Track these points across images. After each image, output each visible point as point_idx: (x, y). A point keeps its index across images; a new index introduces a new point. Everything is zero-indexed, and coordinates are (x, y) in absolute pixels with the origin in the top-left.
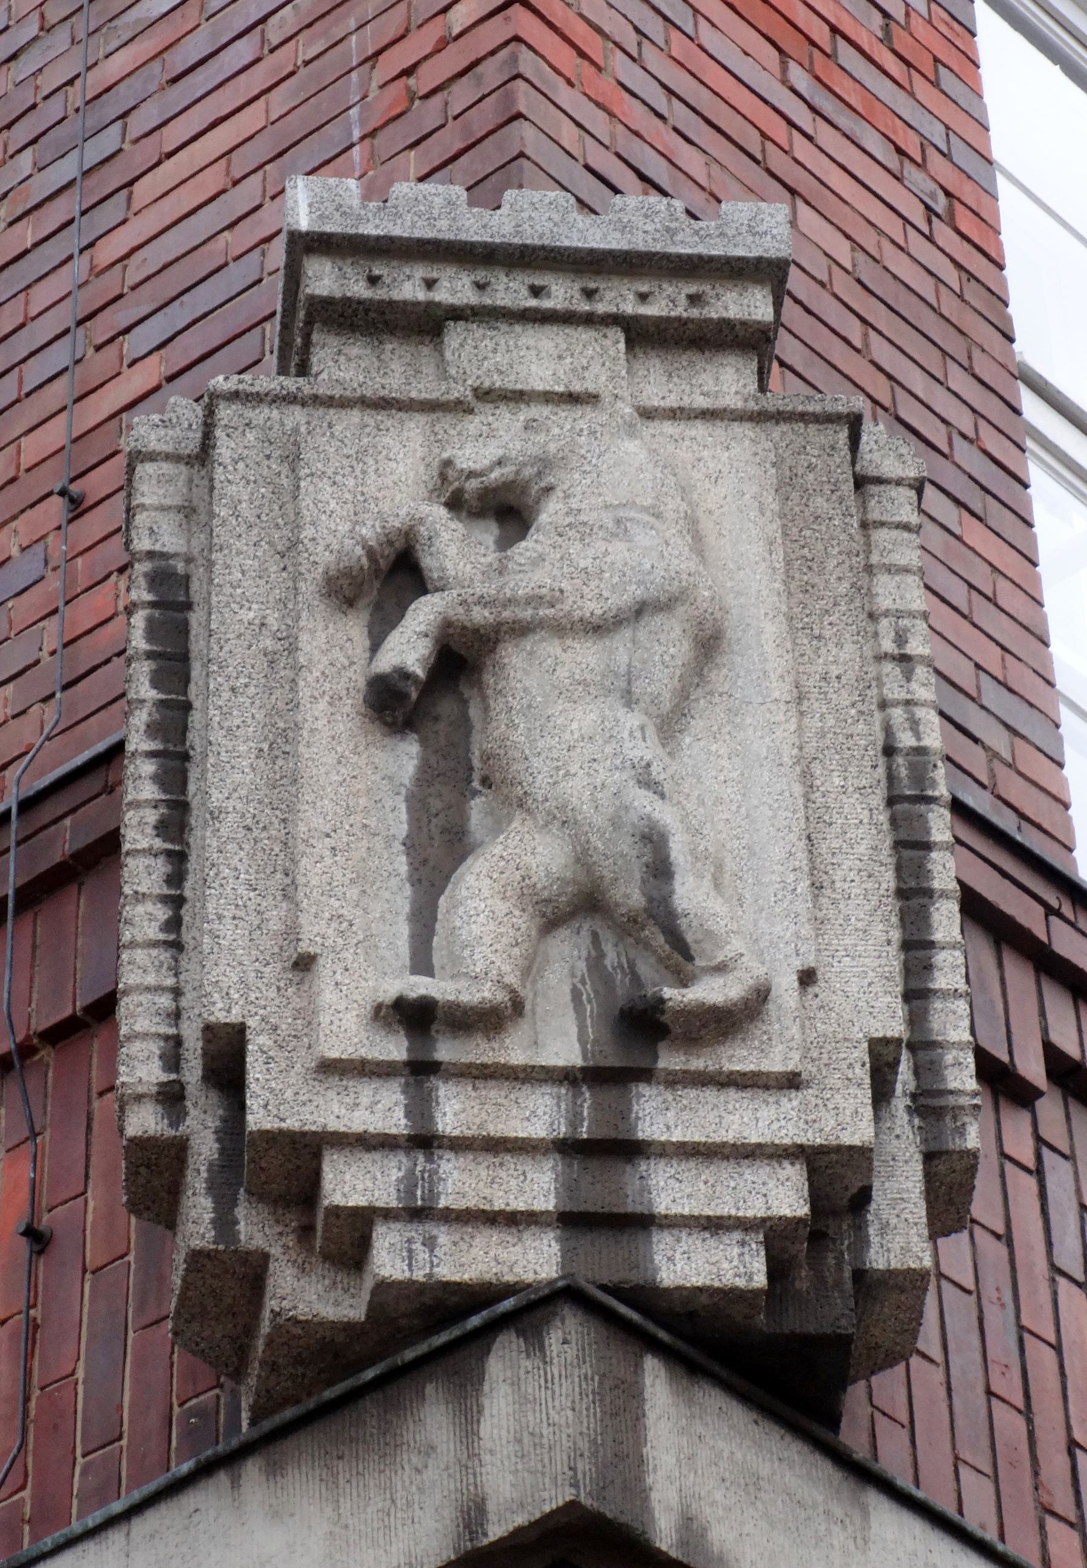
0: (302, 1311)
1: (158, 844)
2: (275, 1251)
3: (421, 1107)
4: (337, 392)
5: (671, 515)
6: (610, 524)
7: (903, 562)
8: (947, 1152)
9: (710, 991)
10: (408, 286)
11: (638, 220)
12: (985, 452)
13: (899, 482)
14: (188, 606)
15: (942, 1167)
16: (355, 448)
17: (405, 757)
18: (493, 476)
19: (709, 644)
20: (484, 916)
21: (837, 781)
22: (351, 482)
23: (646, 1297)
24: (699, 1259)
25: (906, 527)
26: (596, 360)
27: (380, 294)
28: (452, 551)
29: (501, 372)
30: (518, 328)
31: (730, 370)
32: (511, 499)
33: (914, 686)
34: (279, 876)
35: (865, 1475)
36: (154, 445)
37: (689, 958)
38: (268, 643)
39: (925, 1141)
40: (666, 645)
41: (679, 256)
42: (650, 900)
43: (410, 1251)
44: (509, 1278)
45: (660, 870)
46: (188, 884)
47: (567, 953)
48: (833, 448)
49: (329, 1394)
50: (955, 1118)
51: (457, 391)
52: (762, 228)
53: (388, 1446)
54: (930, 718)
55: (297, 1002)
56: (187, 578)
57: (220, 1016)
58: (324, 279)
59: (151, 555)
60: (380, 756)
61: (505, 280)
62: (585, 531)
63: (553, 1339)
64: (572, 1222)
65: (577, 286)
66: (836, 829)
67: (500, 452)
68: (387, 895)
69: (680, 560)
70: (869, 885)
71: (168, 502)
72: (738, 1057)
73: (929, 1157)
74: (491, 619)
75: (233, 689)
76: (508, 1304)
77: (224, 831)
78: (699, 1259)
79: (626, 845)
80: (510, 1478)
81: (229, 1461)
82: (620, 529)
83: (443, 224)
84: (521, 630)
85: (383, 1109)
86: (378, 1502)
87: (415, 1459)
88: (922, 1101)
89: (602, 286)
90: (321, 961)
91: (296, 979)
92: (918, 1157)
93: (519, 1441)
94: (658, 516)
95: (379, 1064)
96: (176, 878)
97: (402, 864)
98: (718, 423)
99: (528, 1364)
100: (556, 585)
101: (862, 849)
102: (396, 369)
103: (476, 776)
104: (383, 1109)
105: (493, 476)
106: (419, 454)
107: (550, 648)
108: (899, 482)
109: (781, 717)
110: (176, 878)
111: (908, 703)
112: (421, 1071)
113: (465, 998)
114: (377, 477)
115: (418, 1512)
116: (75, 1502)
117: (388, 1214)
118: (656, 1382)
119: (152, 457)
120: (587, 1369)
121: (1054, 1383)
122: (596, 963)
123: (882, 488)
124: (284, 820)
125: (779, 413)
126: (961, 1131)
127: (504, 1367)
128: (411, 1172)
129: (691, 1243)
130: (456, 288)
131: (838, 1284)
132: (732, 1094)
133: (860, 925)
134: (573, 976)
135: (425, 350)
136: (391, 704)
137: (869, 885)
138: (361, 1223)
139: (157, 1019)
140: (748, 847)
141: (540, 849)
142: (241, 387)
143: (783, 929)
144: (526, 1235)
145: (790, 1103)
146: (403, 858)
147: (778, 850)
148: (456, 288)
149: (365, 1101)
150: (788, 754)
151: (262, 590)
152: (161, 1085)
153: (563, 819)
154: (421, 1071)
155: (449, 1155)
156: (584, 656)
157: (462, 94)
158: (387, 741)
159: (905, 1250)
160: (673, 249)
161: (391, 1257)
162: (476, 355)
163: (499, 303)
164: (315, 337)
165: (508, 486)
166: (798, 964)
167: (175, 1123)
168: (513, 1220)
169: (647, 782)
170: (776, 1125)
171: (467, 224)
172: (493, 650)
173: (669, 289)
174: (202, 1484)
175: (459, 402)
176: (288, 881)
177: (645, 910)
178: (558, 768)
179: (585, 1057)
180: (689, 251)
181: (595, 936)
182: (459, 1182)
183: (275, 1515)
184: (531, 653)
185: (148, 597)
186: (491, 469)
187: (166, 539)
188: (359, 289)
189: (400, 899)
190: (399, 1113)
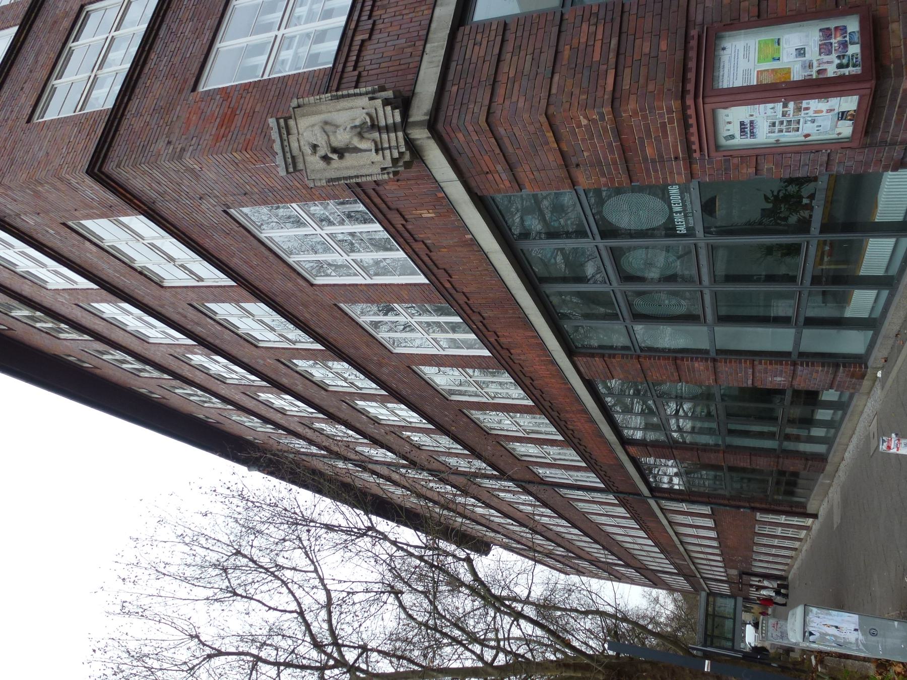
3: (386, 149)
9: (368, 120)
10: (290, 160)
17: (347, 155)
19: (326, 123)
20: (363, 145)
23: (402, 121)
26: (293, 139)
40: (327, 128)
45: (355, 127)
47: (366, 135)
58: (291, 170)
62: (317, 139)
64: (396, 131)
72: (374, 115)
81: (423, 161)
82: (316, 135)
85: (387, 152)
102: (300, 161)
104: (387, 152)
112: (383, 149)
114: (314, 162)
118: (411, 120)
130: (288, 155)
136: (341, 157)
138: (400, 153)
148: (288, 155)
153: (351, 138)
154: (383, 149)
156: (332, 138)
157: (258, 155)
161: (403, 149)
162: (296, 152)
182: (394, 143)
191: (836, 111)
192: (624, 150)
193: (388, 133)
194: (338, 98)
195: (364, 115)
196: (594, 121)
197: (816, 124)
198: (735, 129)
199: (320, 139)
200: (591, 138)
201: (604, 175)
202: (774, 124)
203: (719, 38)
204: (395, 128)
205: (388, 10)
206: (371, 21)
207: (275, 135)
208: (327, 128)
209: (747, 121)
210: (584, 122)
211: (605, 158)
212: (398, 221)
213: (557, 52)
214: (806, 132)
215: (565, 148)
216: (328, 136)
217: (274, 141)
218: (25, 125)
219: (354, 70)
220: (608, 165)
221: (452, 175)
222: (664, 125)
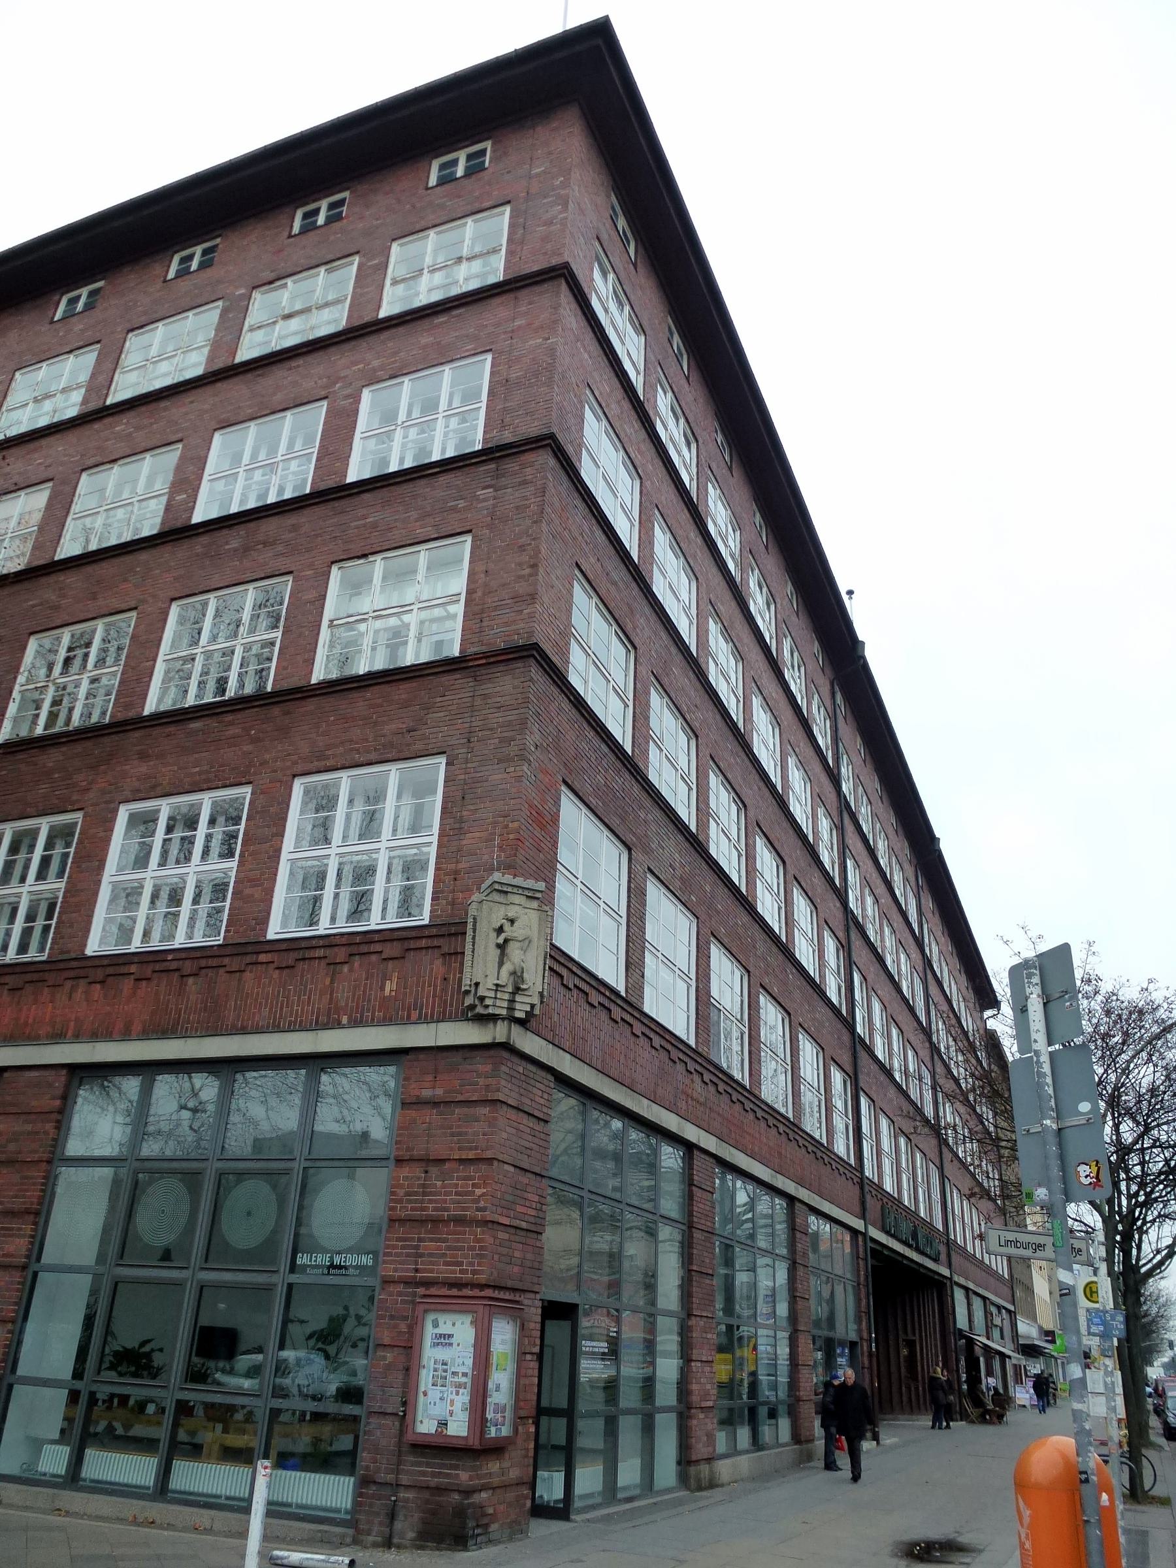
47: (512, 978)
58: (497, 886)
64: (508, 1008)
85: (492, 994)
104: (492, 994)
112: (496, 991)
127: (499, 1022)
130: (510, 889)
136: (498, 946)
147: (533, 969)
148: (510, 889)
154: (496, 991)
156: (518, 944)
161: (491, 1011)
182: (498, 1003)
191: (449, 1418)
192: (436, 1221)
196: (477, 1201)
197: (438, 1401)
198: (444, 1329)
200: (457, 1194)
201: (408, 1194)
202: (444, 1364)
203: (514, 1321)
204: (511, 1009)
207: (530, 883)
209: (452, 1340)
210: (478, 1192)
211: (430, 1201)
212: (390, 950)
213: (526, 1171)
214: (430, 1393)
215: (447, 1165)
218: (576, 558)
220: (422, 1202)
222: (460, 1264)
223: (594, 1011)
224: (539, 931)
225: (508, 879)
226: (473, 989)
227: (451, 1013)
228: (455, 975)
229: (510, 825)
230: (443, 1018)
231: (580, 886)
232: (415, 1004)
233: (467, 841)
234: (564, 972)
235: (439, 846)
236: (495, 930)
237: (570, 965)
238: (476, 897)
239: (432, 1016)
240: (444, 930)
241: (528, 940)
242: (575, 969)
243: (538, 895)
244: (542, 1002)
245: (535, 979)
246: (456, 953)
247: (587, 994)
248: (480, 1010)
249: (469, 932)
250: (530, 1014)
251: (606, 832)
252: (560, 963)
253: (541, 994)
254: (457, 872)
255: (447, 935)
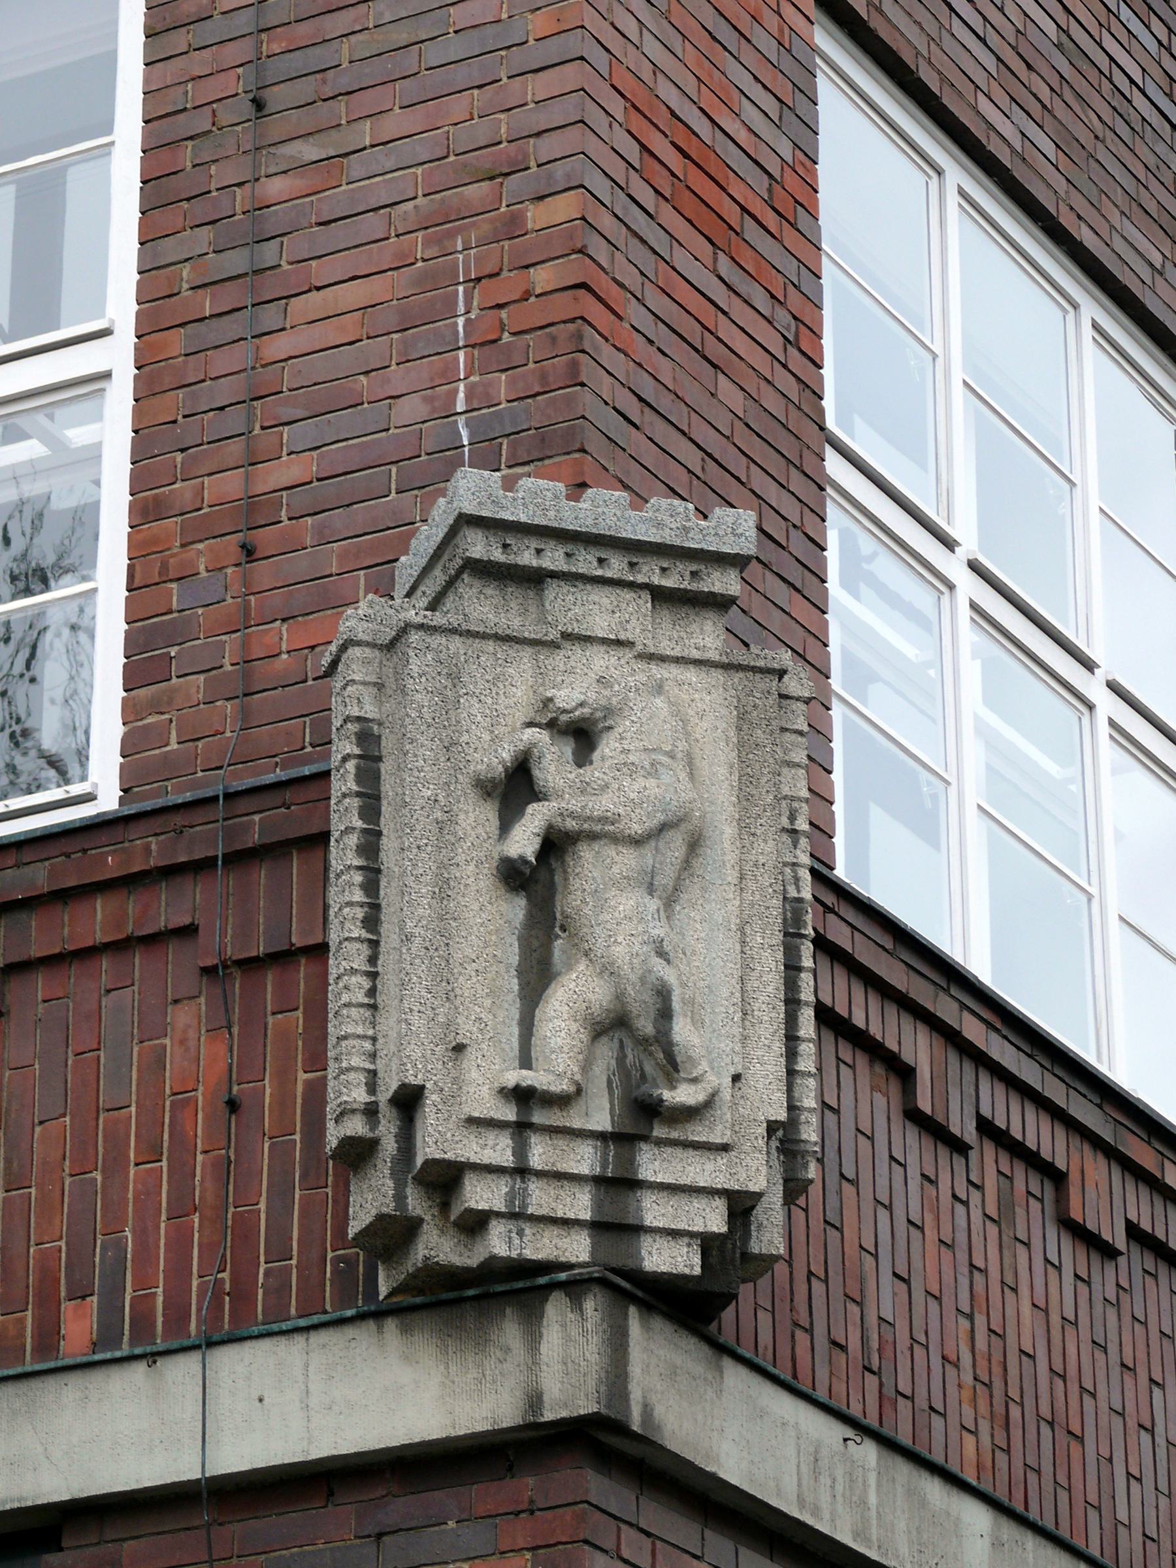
0: (442, 1258)
1: (365, 934)
2: (427, 1218)
3: (521, 1150)
4: (481, 629)
5: (680, 755)
6: (647, 764)
7: (797, 760)
8: (797, 1179)
9: (683, 1095)
11: (668, 520)
12: (806, 534)
13: (798, 699)
14: (379, 759)
15: (791, 1184)
16: (493, 675)
18: (577, 713)
19: (695, 845)
21: (759, 940)
22: (489, 701)
24: (666, 1254)
25: (801, 733)
26: (628, 615)
27: (511, 559)
28: (552, 768)
29: (577, 621)
30: (589, 587)
31: (710, 623)
32: (584, 726)
33: (798, 852)
34: (444, 984)
35: (722, 1349)
36: (361, 636)
37: (678, 1071)
38: (439, 814)
39: (785, 1171)
40: (674, 847)
41: (690, 548)
42: (658, 1032)
43: (510, 1238)
44: (563, 1259)
45: (665, 1014)
46: (379, 963)
47: (606, 1052)
48: (769, 692)
49: (444, 1296)
50: (803, 1157)
51: (553, 635)
52: (740, 531)
53: (481, 1343)
54: (806, 875)
55: (454, 1073)
56: (379, 737)
57: (411, 1080)
58: (478, 546)
59: (359, 719)
60: (504, 907)
61: (584, 553)
63: (589, 1305)
64: (598, 1227)
65: (626, 560)
66: (756, 974)
67: (583, 697)
68: (506, 1006)
69: (687, 792)
70: (773, 1015)
71: (368, 679)
72: (698, 1132)
73: (786, 1181)
74: (577, 827)
75: (419, 847)
76: (563, 1276)
77: (413, 950)
78: (666, 1254)
79: (648, 996)
80: (559, 1385)
82: (653, 771)
83: (552, 514)
84: (593, 837)
85: (497, 1150)
86: (473, 1374)
87: (498, 1353)
88: (786, 1146)
89: (641, 561)
90: (469, 1049)
91: (454, 1057)
92: (781, 1181)
93: (565, 1364)
94: (673, 757)
95: (500, 1121)
96: (373, 960)
97: (515, 985)
98: (703, 668)
99: (570, 1315)
100: (616, 811)
101: (770, 989)
103: (558, 924)
105: (577, 713)
106: (530, 683)
107: (610, 851)
108: (798, 699)
109: (731, 896)
110: (373, 960)
111: (794, 864)
112: (521, 1129)
113: (553, 1088)
114: (499, 711)
115: (500, 1388)
116: (260, 1291)
117: (498, 1215)
119: (359, 643)
120: (605, 1326)
121: (803, 1238)
122: (621, 1060)
123: (788, 701)
124: (447, 944)
125: (740, 665)
126: (805, 1166)
127: (556, 1309)
128: (513, 1188)
129: (661, 1242)
130: (554, 558)
131: (733, 1260)
132: (691, 1152)
133: (766, 1042)
134: (609, 1069)
135: (531, 594)
136: (514, 876)
137: (773, 1015)
139: (363, 1058)
140: (708, 987)
141: (597, 989)
142: (425, 621)
143: (725, 1045)
144: (572, 1231)
145: (722, 1160)
146: (516, 981)
147: (726, 990)
148: (554, 558)
149: (491, 1143)
150: (735, 921)
151: (435, 775)
152: (366, 1104)
153: (608, 970)
154: (521, 1129)
155: (534, 1179)
156: (625, 860)
158: (508, 895)
159: (771, 1242)
160: (686, 544)
161: (500, 1242)
163: (580, 571)
164: (465, 576)
165: (583, 719)
166: (733, 1070)
167: (372, 1129)
168: (566, 1223)
169: (661, 954)
170: (713, 1176)
171: (566, 514)
172: (574, 844)
173: (681, 566)
174: (358, 1323)
175: (552, 642)
176: (449, 988)
177: (655, 1037)
178: (610, 936)
179: (613, 1127)
180: (696, 546)
181: (621, 1041)
183: (406, 1358)
184: (598, 853)
185: (357, 751)
186: (576, 709)
187: (368, 707)
188: (498, 555)
189: (512, 1010)
190: (509, 1152)
193: (599, 1181)
194: (791, 936)
195: (712, 1080)
199: (634, 787)
205: (993, 1230)
206: (969, 1133)
207: (664, 519)
208: (674, 847)
216: (637, 842)
217: (639, 500)
219: (1133, 1231)
221: (242, 1452)
223: (1105, 1279)
224: (745, 798)
225: (537, 497)
226: (387, 1131)
227: (278, 1291)
228: (284, 1077)
229: (535, 216)
230: (232, 1320)
231: (968, 586)
232: (79, 1256)
233: (297, 337)
234: (917, 1047)
235: (147, 391)
236: (485, 788)
237: (946, 1008)
238: (364, 617)
239: (177, 1315)
240: (206, 838)
241: (678, 837)
242: (973, 1030)
243: (725, 582)
244: (794, 1189)
245: (739, 1049)
246: (283, 957)
247: (1056, 1177)
248: (437, 1246)
249: (345, 817)
250: (727, 1254)
251: (1093, 308)
252: (876, 985)
253: (784, 1137)
254: (254, 511)
255: (235, 851)
